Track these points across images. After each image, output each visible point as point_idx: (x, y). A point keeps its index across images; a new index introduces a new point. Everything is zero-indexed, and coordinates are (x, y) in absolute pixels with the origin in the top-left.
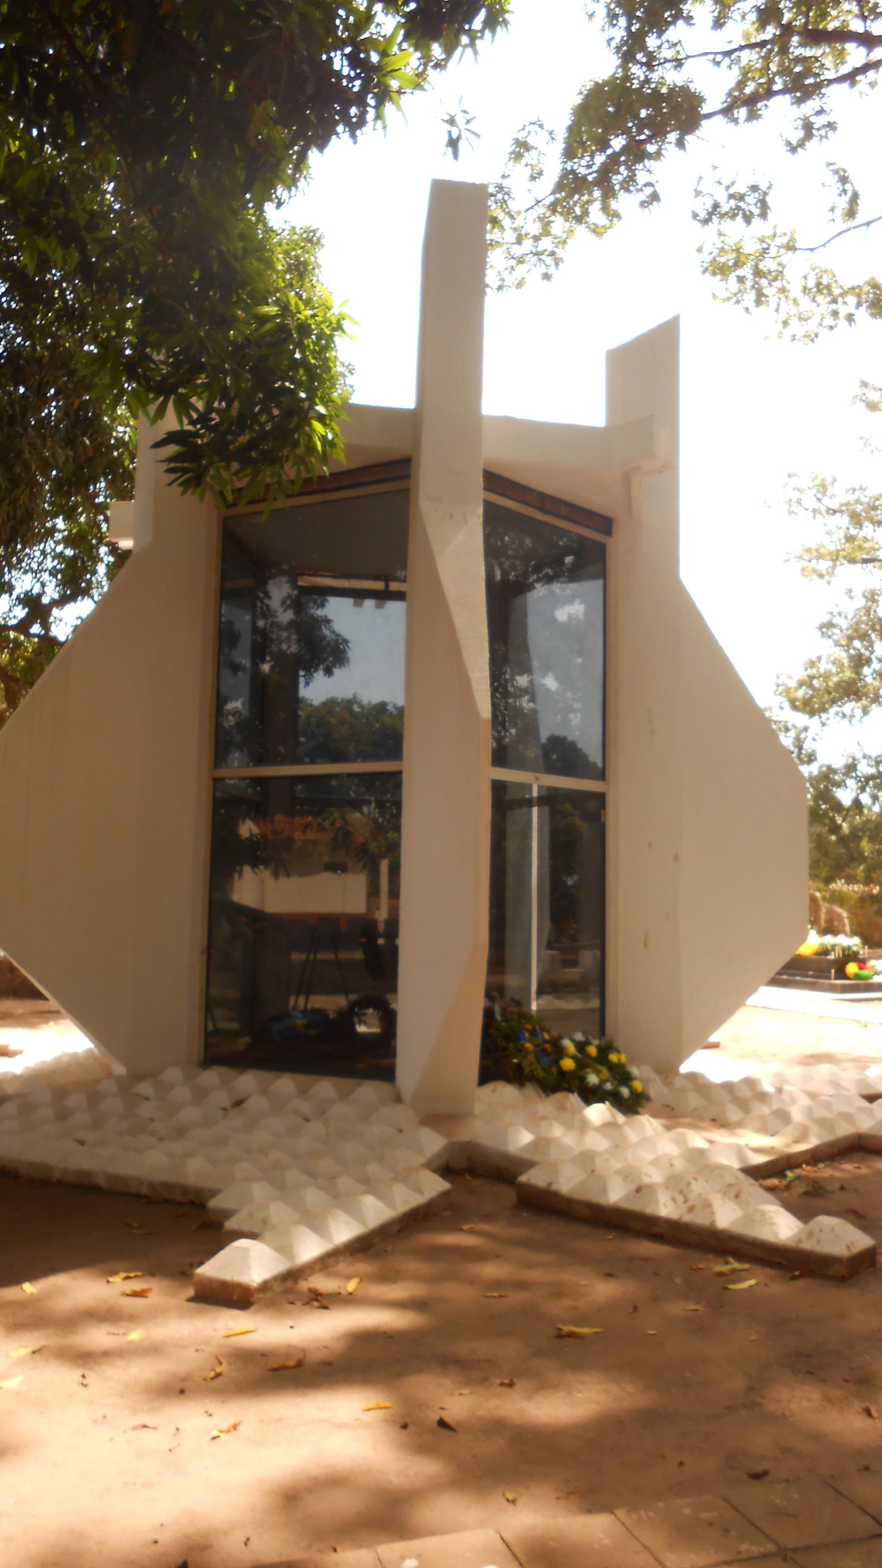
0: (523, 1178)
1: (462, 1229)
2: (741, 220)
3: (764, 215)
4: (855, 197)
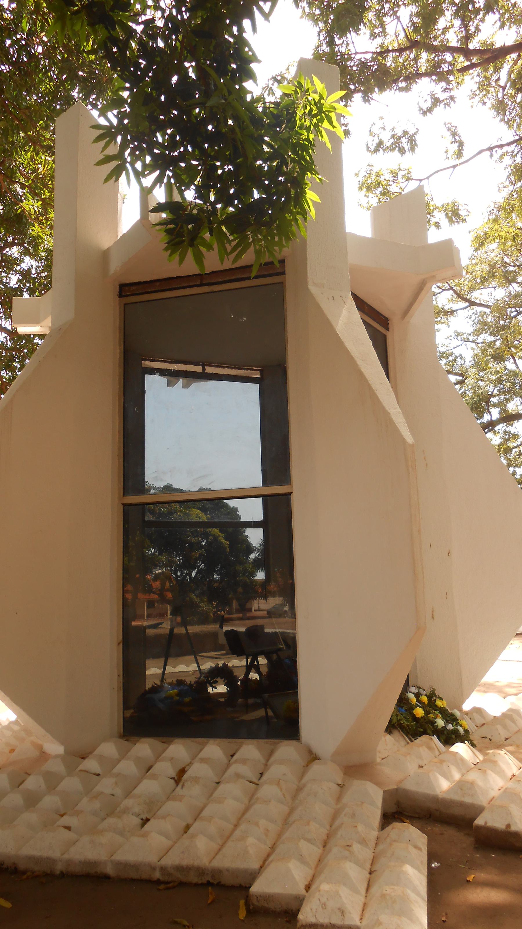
0: (479, 821)
1: (469, 881)
2: (397, 152)
3: (412, 149)
4: (461, 144)
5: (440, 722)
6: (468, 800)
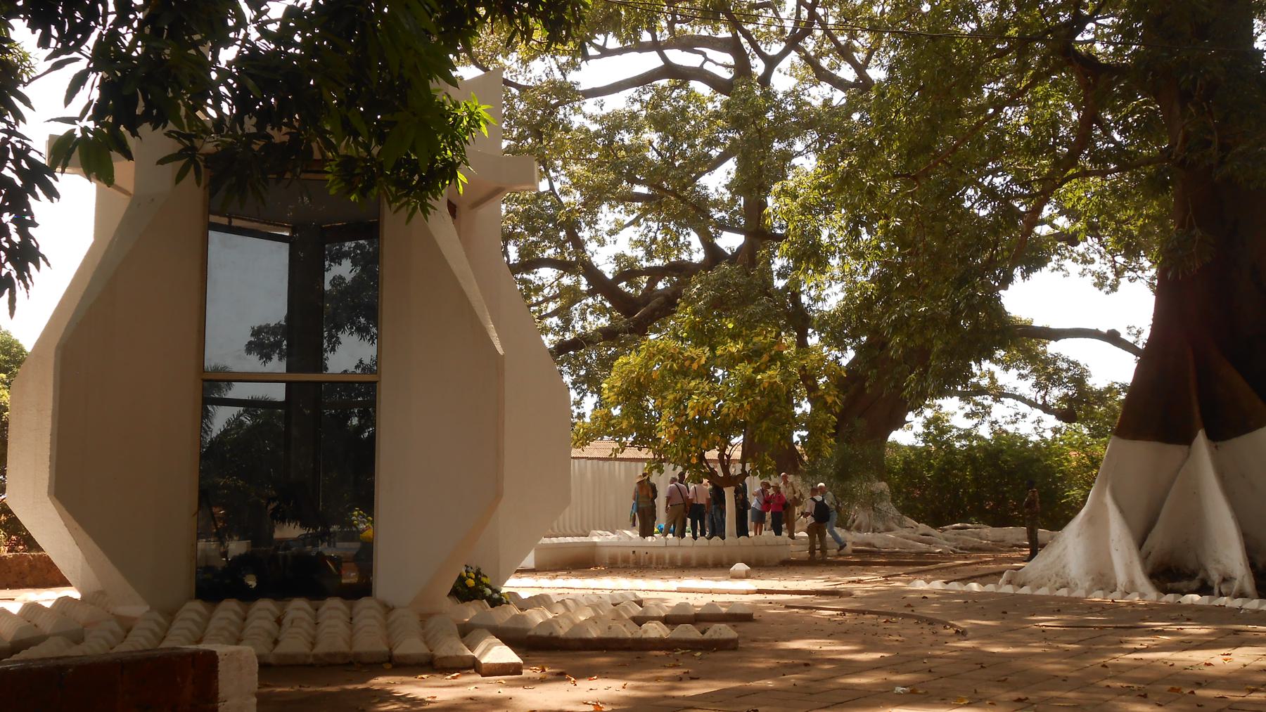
5: (488, 591)
6: (521, 626)
